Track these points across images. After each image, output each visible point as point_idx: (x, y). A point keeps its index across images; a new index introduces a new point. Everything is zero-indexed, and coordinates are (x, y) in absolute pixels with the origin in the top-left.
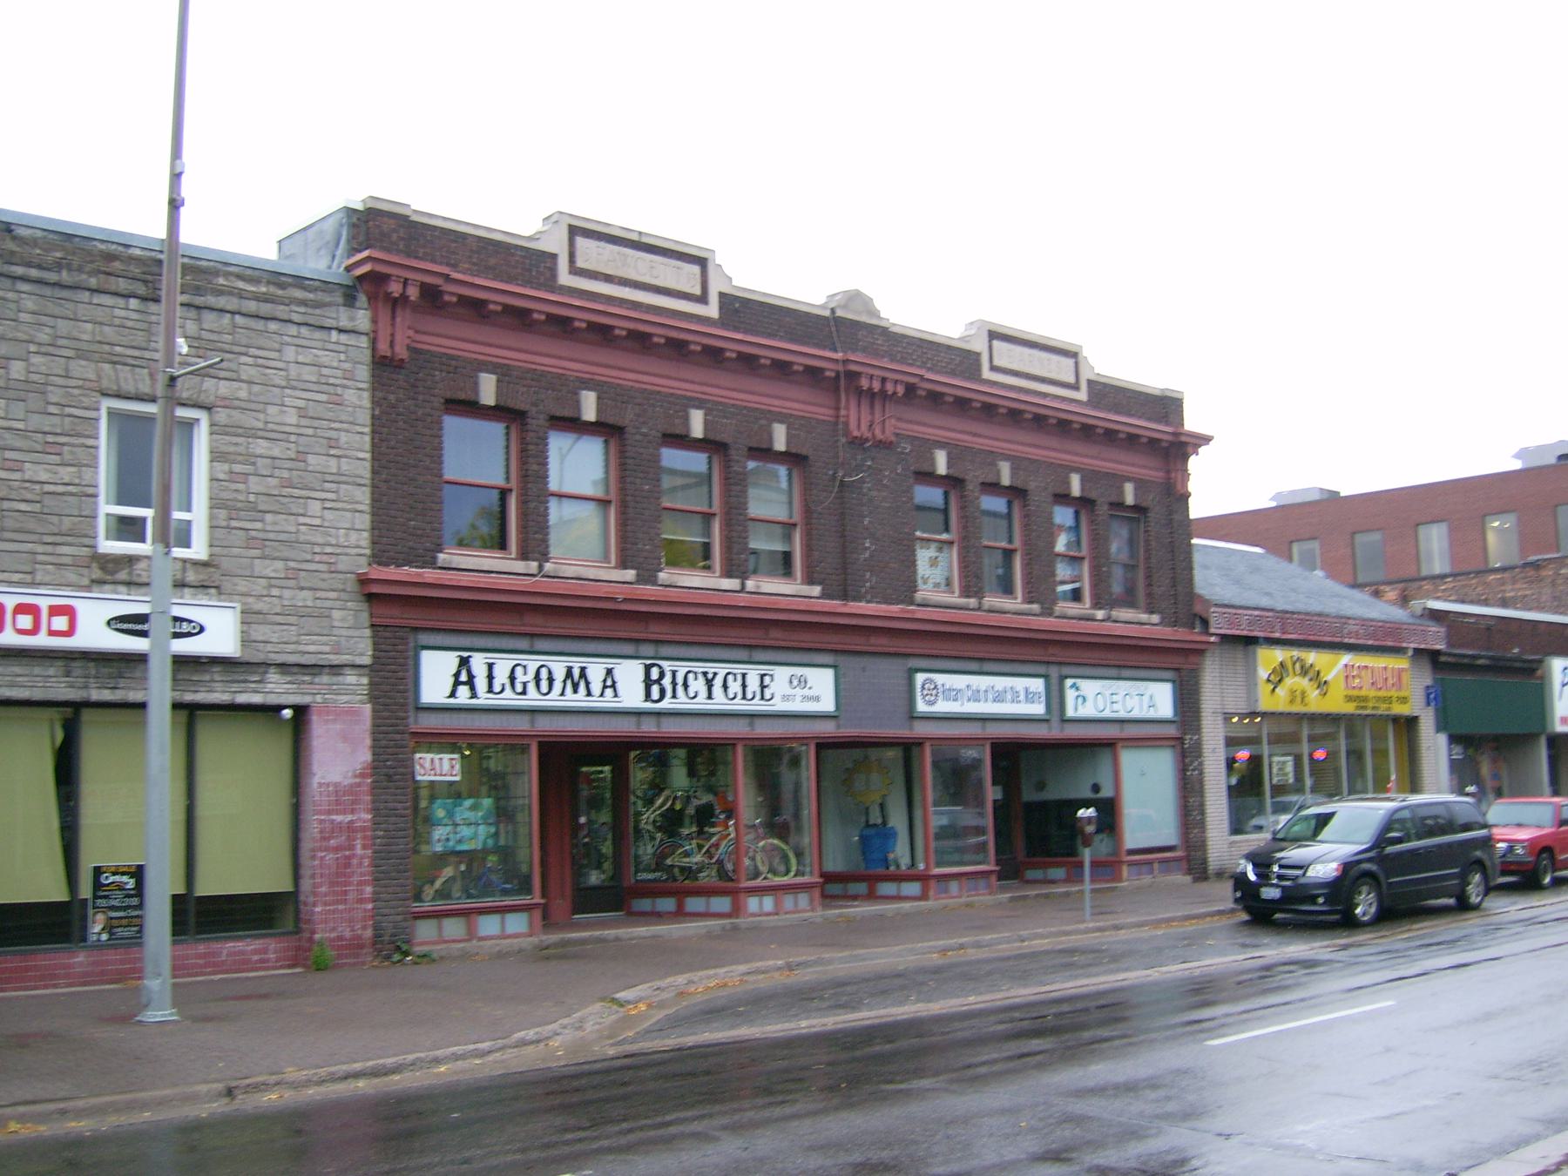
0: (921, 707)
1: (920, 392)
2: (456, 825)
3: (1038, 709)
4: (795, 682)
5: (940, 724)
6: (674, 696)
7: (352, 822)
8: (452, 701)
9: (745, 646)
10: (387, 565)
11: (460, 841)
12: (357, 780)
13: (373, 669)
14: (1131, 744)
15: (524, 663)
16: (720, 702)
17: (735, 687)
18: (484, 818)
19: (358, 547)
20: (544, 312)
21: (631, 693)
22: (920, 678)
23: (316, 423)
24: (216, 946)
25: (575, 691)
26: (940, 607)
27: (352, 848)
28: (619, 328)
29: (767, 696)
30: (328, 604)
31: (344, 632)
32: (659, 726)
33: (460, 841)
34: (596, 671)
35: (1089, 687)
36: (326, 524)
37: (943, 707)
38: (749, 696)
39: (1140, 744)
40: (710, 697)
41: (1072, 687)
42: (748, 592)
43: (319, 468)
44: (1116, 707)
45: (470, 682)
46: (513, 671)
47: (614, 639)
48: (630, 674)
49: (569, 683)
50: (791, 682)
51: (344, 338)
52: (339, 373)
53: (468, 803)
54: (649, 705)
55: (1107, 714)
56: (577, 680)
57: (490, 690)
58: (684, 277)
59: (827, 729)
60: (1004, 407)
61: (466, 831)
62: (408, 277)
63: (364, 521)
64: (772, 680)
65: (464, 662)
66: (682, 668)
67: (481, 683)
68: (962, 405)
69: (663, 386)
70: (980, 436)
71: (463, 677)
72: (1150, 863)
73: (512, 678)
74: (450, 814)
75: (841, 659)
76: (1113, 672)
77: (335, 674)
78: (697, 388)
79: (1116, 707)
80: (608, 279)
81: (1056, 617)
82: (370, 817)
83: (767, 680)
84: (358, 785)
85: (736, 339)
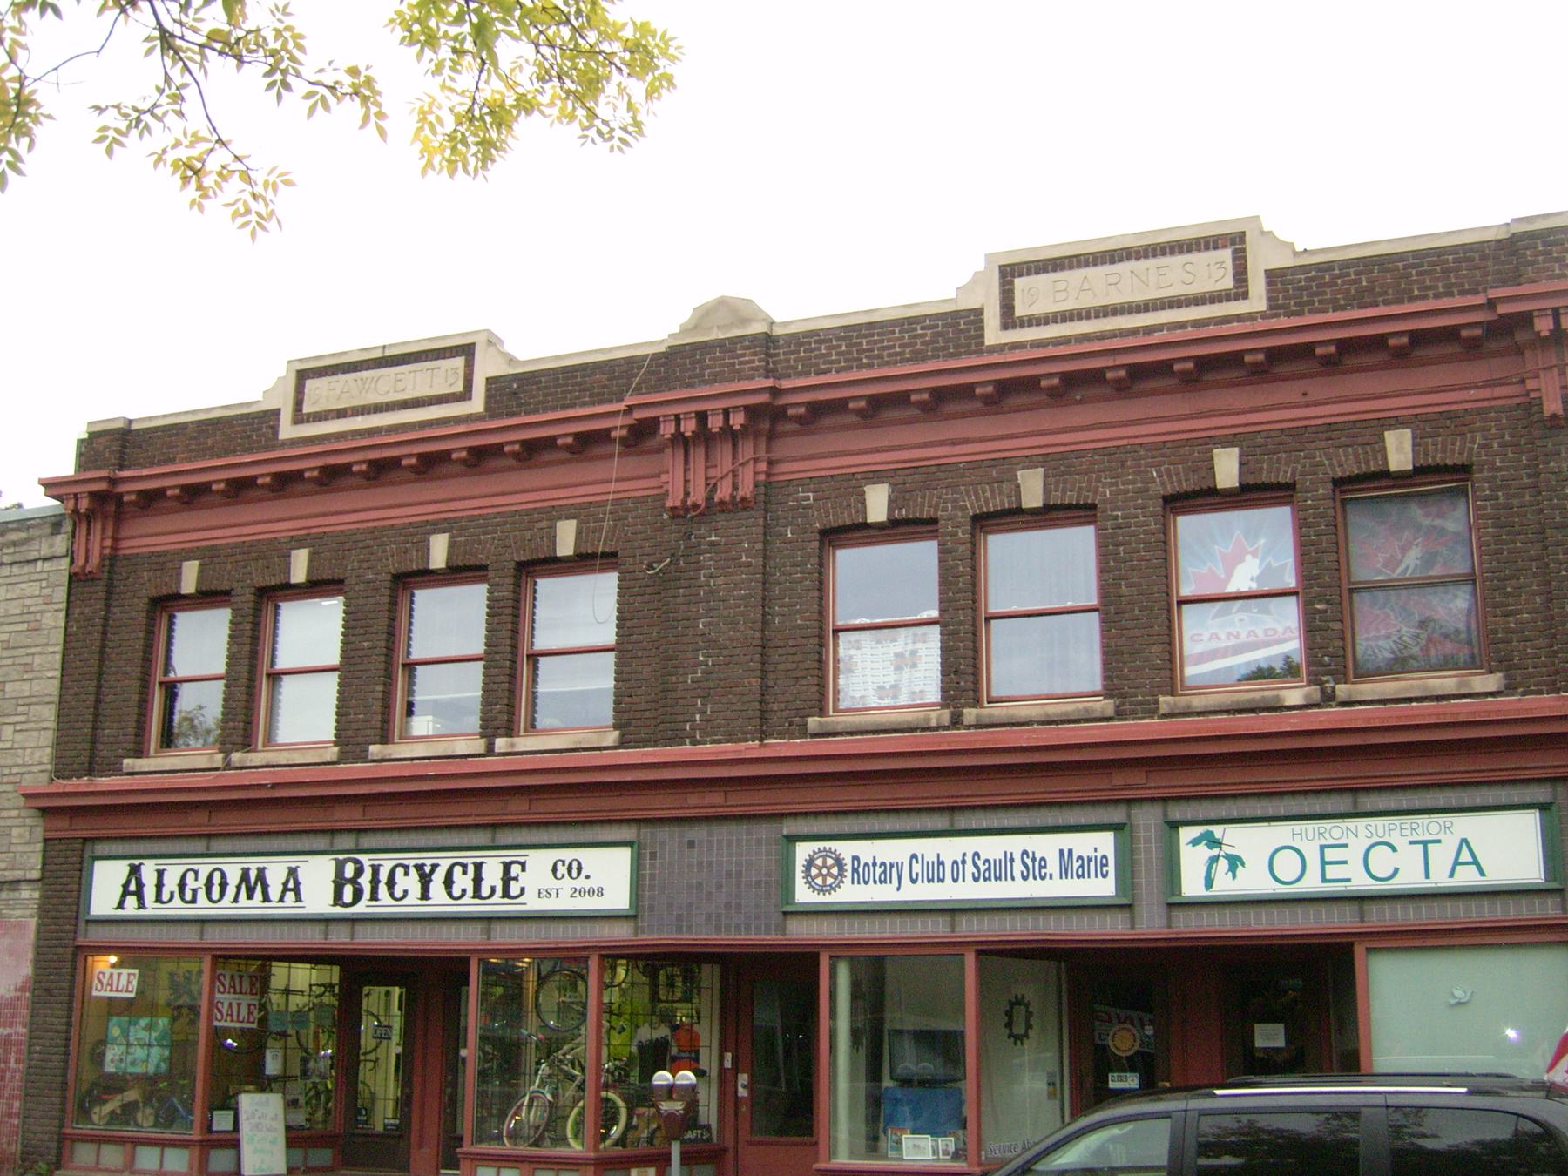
0: (804, 894)
2: (129, 1045)
3: (1103, 887)
4: (562, 870)
6: (374, 897)
7: (9, 1035)
8: (120, 912)
10: (69, 777)
11: (133, 1064)
12: (18, 994)
13: (47, 878)
15: (196, 867)
17: (463, 882)
18: (159, 1040)
19: (41, 763)
20: (222, 481)
21: (317, 897)
22: (803, 850)
23: (15, 652)
28: (170, 488)
30: (9, 822)
31: (20, 848)
32: (326, 934)
33: (133, 1064)
34: (276, 872)
35: (1243, 839)
36: (16, 746)
37: (850, 893)
38: (485, 891)
40: (425, 895)
41: (1195, 842)
42: (373, 761)
43: (14, 694)
44: (1332, 872)
45: (139, 894)
46: (184, 877)
47: (1397, 787)
48: (317, 873)
49: (243, 887)
50: (554, 870)
51: (48, 566)
52: (40, 600)
53: (144, 1022)
54: (339, 910)
55: (1312, 884)
56: (252, 884)
57: (159, 899)
58: (1213, 271)
59: (621, 933)
61: (139, 1053)
62: (1557, 305)
63: (48, 737)
64: (523, 870)
65: (135, 871)
66: (386, 863)
67: (149, 893)
68: (285, 483)
70: (966, 441)
71: (133, 887)
74: (125, 1033)
76: (1344, 803)
77: (14, 890)
78: (443, 507)
79: (1332, 872)
80: (341, 414)
81: (1165, 716)
82: (24, 1030)
83: (515, 870)
84: (18, 998)
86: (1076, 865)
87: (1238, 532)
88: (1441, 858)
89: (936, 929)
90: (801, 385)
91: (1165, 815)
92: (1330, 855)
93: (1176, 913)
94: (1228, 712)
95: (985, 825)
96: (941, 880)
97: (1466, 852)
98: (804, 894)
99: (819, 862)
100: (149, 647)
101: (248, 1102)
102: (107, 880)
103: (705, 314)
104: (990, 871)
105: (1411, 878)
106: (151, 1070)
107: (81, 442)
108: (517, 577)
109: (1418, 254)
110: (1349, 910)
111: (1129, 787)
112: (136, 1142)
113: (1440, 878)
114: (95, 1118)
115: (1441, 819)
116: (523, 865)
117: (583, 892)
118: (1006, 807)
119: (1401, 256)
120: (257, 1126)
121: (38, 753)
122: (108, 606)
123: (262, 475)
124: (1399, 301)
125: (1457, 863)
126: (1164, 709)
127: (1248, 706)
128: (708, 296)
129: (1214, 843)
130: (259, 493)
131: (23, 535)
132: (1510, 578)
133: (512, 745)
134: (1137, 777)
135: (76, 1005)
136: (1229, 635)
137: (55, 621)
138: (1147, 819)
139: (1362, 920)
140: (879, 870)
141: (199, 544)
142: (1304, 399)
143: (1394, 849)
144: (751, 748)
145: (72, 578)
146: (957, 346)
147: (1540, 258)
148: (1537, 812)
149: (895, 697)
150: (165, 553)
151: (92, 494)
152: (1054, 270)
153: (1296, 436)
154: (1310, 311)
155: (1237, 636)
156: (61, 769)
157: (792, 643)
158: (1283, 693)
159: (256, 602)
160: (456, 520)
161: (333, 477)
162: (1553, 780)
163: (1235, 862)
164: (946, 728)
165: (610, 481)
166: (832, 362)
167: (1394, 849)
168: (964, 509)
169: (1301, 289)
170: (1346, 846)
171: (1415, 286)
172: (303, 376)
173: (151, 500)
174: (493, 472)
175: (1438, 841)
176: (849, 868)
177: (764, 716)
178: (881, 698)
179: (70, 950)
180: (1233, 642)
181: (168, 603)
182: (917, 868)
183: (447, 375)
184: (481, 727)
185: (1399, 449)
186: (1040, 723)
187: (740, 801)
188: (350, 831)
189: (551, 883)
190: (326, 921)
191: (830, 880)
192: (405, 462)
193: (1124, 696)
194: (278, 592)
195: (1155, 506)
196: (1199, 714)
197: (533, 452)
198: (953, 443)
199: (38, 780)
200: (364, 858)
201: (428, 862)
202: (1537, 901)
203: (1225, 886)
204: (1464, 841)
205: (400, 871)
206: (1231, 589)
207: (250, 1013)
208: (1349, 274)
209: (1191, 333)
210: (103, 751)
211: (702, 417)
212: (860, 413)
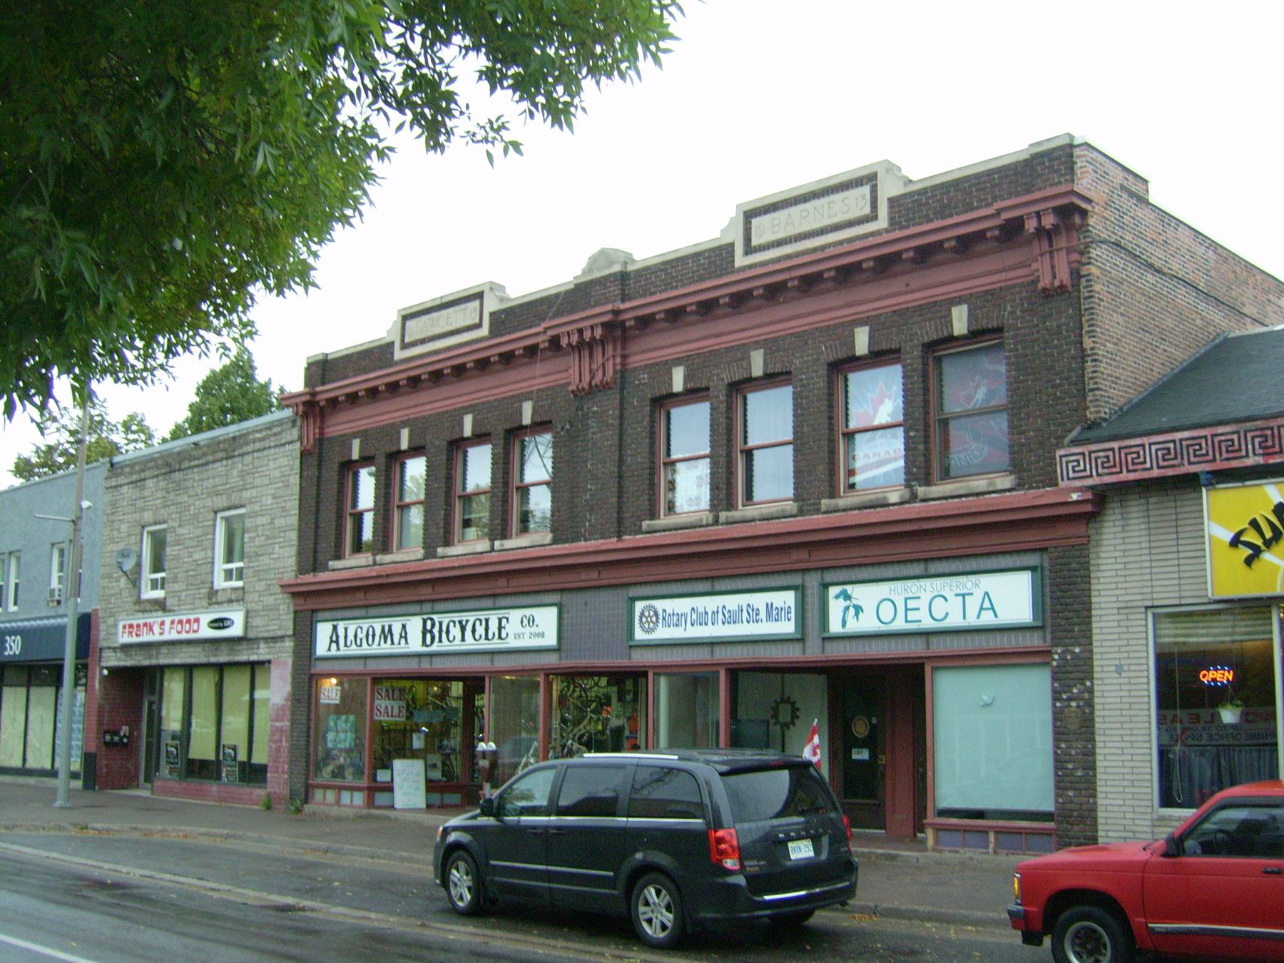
0: (639, 635)
1: (447, 371)
3: (787, 627)
4: (525, 621)
5: (685, 650)
9: (707, 578)
13: (296, 634)
14: (961, 663)
16: (470, 644)
17: (480, 630)
20: (760, 287)
24: (253, 790)
25: (385, 642)
26: (670, 530)
27: (281, 741)
28: (864, 260)
29: (503, 635)
35: (866, 594)
38: (490, 636)
39: (968, 663)
40: (463, 639)
41: (837, 597)
44: (911, 616)
45: (337, 642)
50: (522, 622)
53: (344, 717)
54: (425, 649)
55: (900, 625)
56: (387, 634)
57: (346, 645)
59: (552, 660)
60: (659, 312)
61: (342, 735)
63: (293, 551)
65: (335, 628)
66: (446, 619)
68: (740, 301)
69: (908, 302)
70: (722, 334)
72: (983, 831)
73: (356, 636)
75: (566, 598)
76: (917, 569)
79: (911, 616)
81: (826, 512)
83: (504, 621)
85: (516, 340)
86: (774, 613)
87: (881, 383)
88: (973, 604)
89: (702, 655)
90: (633, 307)
91: (822, 579)
92: (911, 604)
93: (828, 645)
94: (859, 508)
95: (779, 584)
96: (706, 624)
97: (988, 603)
98: (639, 635)
99: (646, 614)
100: (653, 435)
101: (398, 764)
102: (323, 631)
103: (594, 261)
104: (731, 618)
105: (955, 620)
106: (348, 746)
107: (306, 369)
108: (729, 396)
109: (978, 176)
110: (920, 641)
111: (801, 561)
112: (341, 788)
113: (972, 620)
114: (324, 774)
115: (973, 578)
116: (507, 619)
117: (534, 635)
118: (762, 574)
119: (966, 179)
120: (405, 780)
121: (290, 560)
122: (320, 470)
123: (690, 305)
124: (966, 211)
125: (982, 608)
126: (823, 508)
127: (869, 504)
128: (594, 250)
129: (847, 597)
130: (864, 276)
131: (279, 429)
132: (1024, 406)
133: (502, 545)
134: (803, 554)
135: (313, 709)
136: (874, 454)
137: (295, 480)
138: (813, 581)
139: (928, 648)
140: (675, 618)
141: (818, 325)
142: (908, 288)
143: (946, 600)
144: (612, 542)
145: (302, 454)
146: (722, 269)
147: (1046, 171)
148: (1030, 573)
149: (698, 504)
150: (345, 435)
151: (604, 325)
152: (774, 211)
153: (902, 314)
154: (913, 225)
155: (879, 455)
156: (302, 570)
157: (636, 473)
158: (889, 495)
159: (828, 376)
160: (476, 405)
161: (774, 292)
162: (562, 590)
163: (858, 609)
164: (712, 525)
165: (535, 378)
166: (657, 286)
167: (946, 600)
168: (722, 380)
169: (908, 209)
170: (919, 598)
171: (975, 200)
172: (406, 318)
173: (645, 322)
174: (897, 275)
175: (972, 594)
176: (661, 617)
177: (620, 520)
178: (691, 506)
179: (307, 676)
180: (876, 459)
181: (664, 402)
182: (694, 616)
183: (466, 315)
184: (905, 480)
185: (960, 319)
186: (760, 520)
187: (609, 576)
188: (816, 569)
189: (520, 629)
190: (419, 656)
191: (651, 625)
192: (904, 256)
193: (803, 500)
194: (741, 387)
195: (823, 371)
196: (844, 510)
197: (508, 359)
198: (716, 336)
199: (289, 577)
200: (435, 617)
201: (464, 619)
202: (1028, 635)
203: (854, 626)
204: (987, 593)
205: (452, 624)
206: (876, 422)
207: (400, 711)
208: (936, 196)
209: (846, 248)
210: (321, 558)
211: (580, 331)
212: (954, 250)
